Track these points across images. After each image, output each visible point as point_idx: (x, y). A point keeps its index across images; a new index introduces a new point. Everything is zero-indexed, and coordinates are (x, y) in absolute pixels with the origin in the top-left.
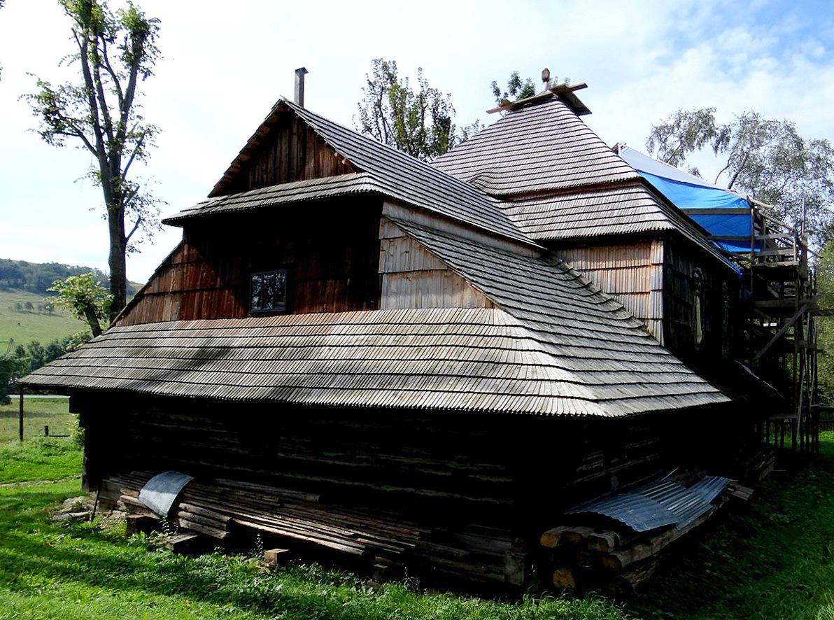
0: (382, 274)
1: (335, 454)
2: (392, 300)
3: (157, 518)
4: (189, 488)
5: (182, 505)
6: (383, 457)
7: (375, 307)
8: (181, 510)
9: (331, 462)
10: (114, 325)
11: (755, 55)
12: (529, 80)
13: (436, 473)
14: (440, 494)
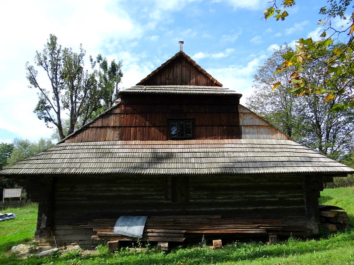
0: (241, 126)
1: (223, 197)
2: (248, 136)
3: (129, 240)
4: (147, 221)
5: (148, 230)
6: (247, 196)
7: (240, 138)
8: (149, 232)
9: (220, 201)
10: (63, 142)
11: (131, 63)
12: (105, 58)
13: (271, 199)
14: (274, 207)
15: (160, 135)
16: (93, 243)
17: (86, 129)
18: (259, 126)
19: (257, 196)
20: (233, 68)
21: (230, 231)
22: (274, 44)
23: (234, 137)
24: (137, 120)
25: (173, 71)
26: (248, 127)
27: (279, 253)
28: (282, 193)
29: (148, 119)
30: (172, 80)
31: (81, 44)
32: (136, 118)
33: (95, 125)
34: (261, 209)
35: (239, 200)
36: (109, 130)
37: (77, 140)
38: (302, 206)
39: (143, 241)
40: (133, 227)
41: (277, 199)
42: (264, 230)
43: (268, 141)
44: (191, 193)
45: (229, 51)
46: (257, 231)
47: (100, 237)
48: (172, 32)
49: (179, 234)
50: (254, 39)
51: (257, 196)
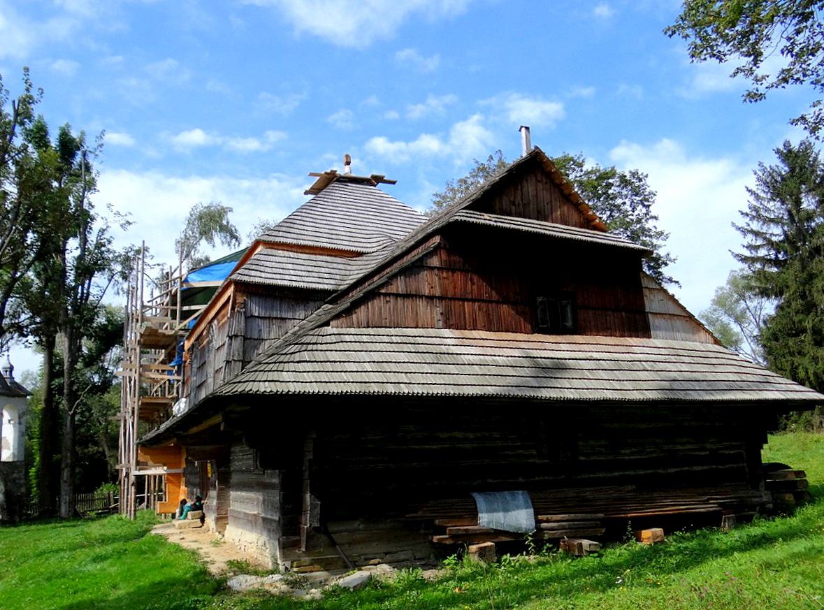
0: (647, 313)
3: (509, 539)
6: (666, 447)
7: (649, 337)
9: (627, 458)
15: (520, 321)
16: (415, 557)
17: (373, 298)
18: (674, 315)
19: (680, 447)
20: (280, 180)
21: (669, 510)
22: (380, 135)
23: (640, 333)
24: (475, 286)
25: (521, 188)
26: (658, 316)
27: (755, 542)
28: (714, 440)
29: (494, 286)
30: (521, 207)
31: (27, 70)
32: (471, 280)
33: (392, 289)
34: (687, 471)
35: (654, 455)
36: (421, 304)
37: (358, 322)
38: (741, 465)
39: (541, 542)
40: (513, 512)
41: (707, 453)
42: (716, 505)
43: (689, 345)
44: (580, 443)
45: (273, 136)
46: (702, 509)
47: (453, 537)
48: (120, 58)
49: (593, 522)
50: (335, 116)
51: (680, 447)
